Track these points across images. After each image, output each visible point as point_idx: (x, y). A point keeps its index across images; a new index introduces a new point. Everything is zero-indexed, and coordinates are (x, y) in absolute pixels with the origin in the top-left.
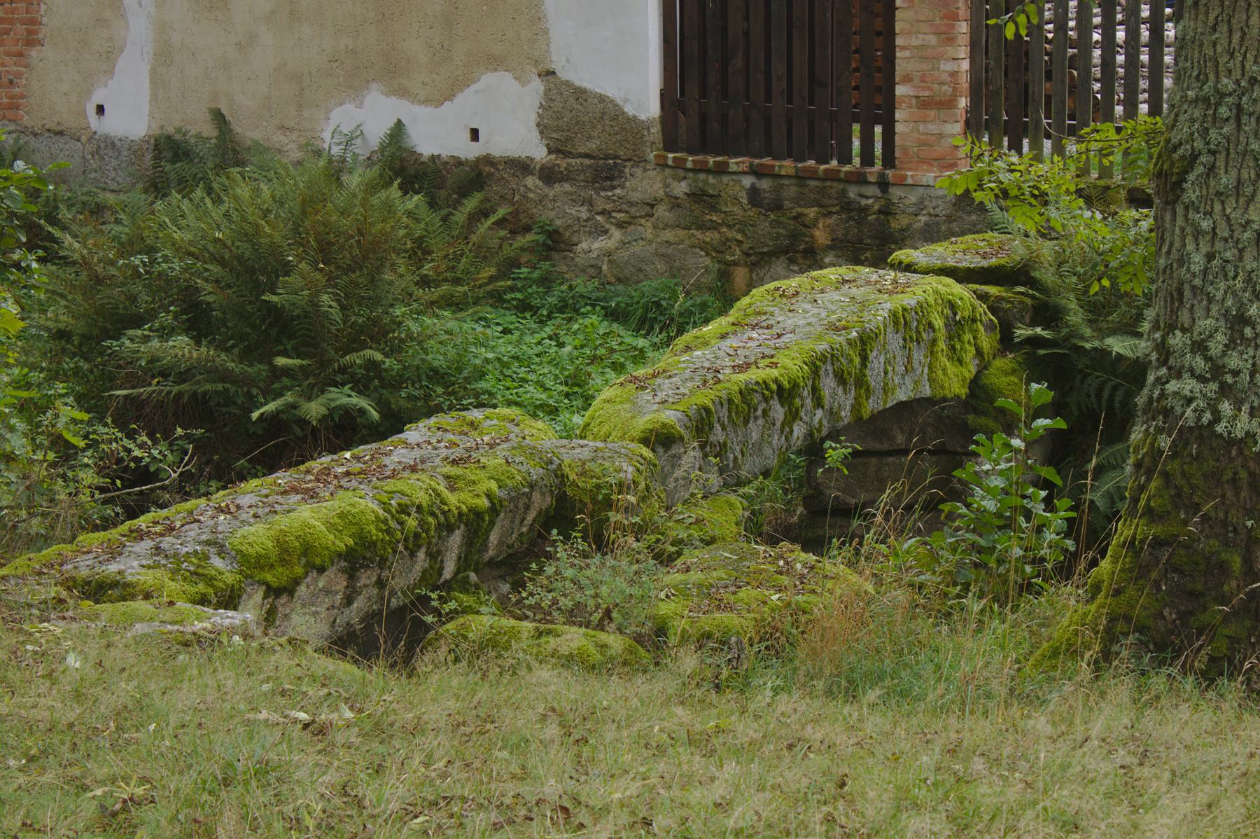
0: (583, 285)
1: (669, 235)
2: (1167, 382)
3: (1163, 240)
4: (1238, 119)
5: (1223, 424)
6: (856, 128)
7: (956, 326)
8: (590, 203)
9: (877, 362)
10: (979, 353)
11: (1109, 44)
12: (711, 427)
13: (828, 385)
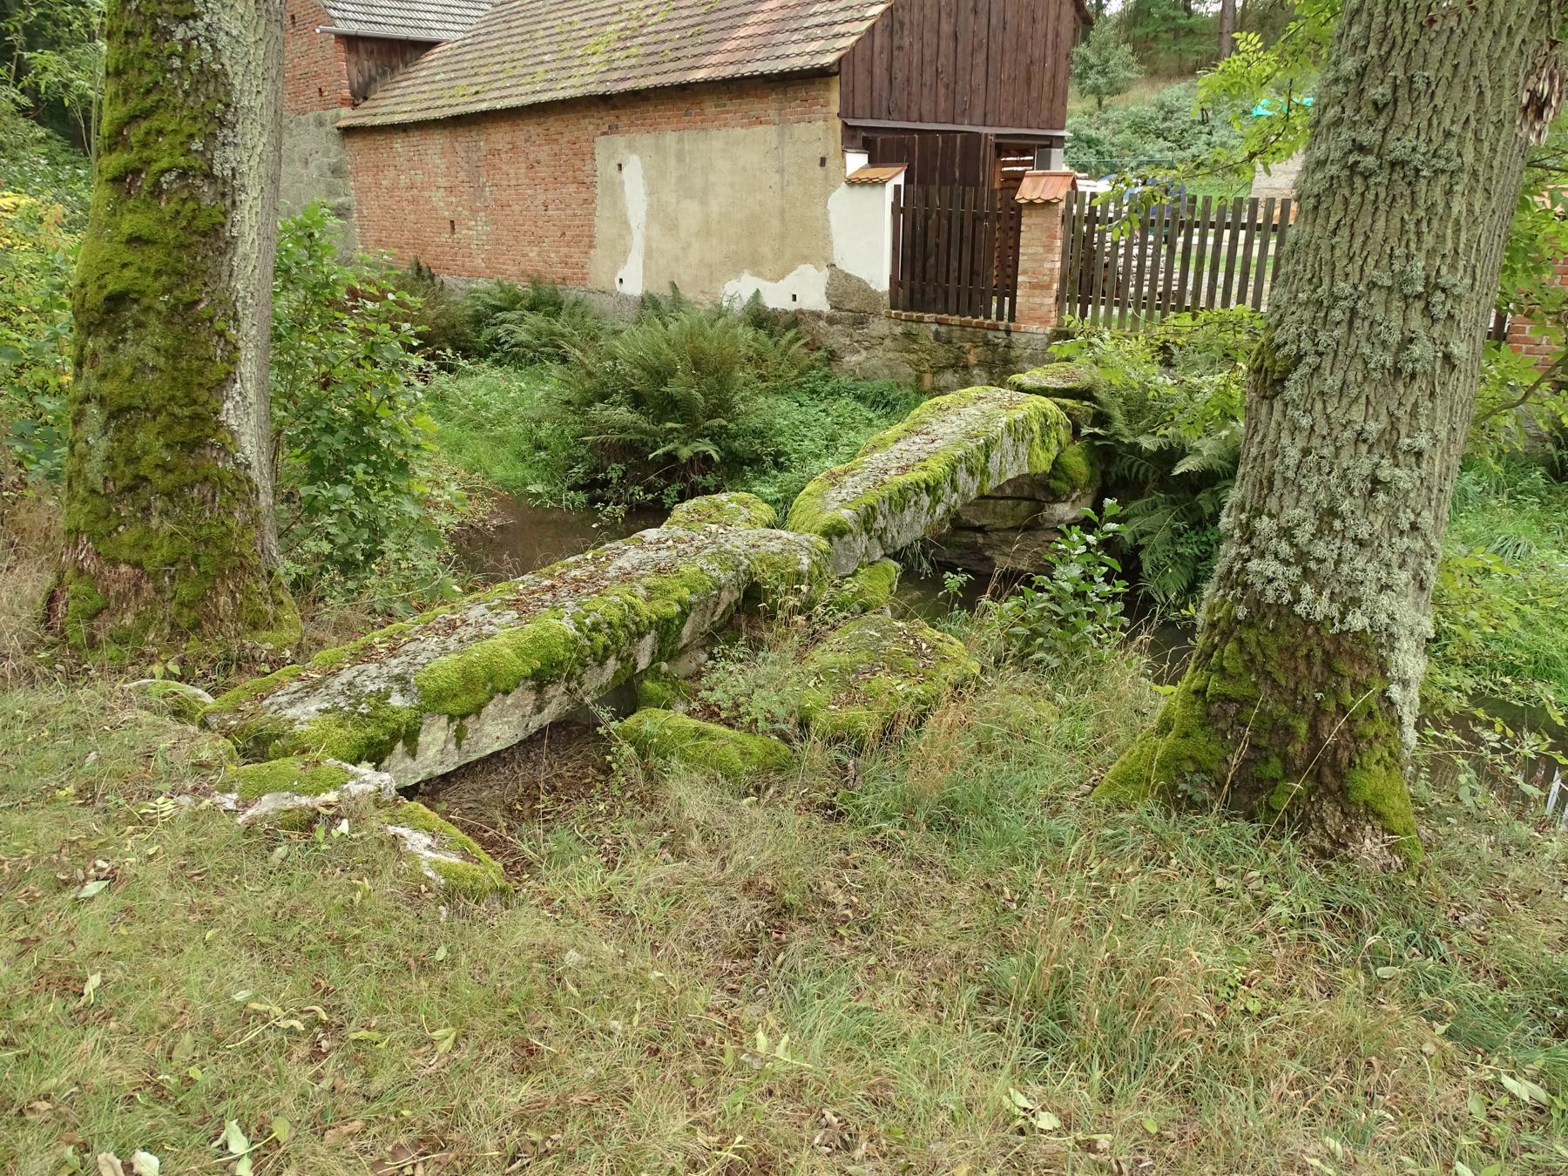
0: (845, 380)
1: (891, 355)
2: (1249, 560)
3: (1256, 430)
4: (1351, 323)
5: (1303, 605)
6: (995, 298)
7: (1046, 428)
8: (851, 336)
9: (995, 456)
10: (1059, 443)
11: (1128, 256)
12: (875, 519)
13: (962, 476)
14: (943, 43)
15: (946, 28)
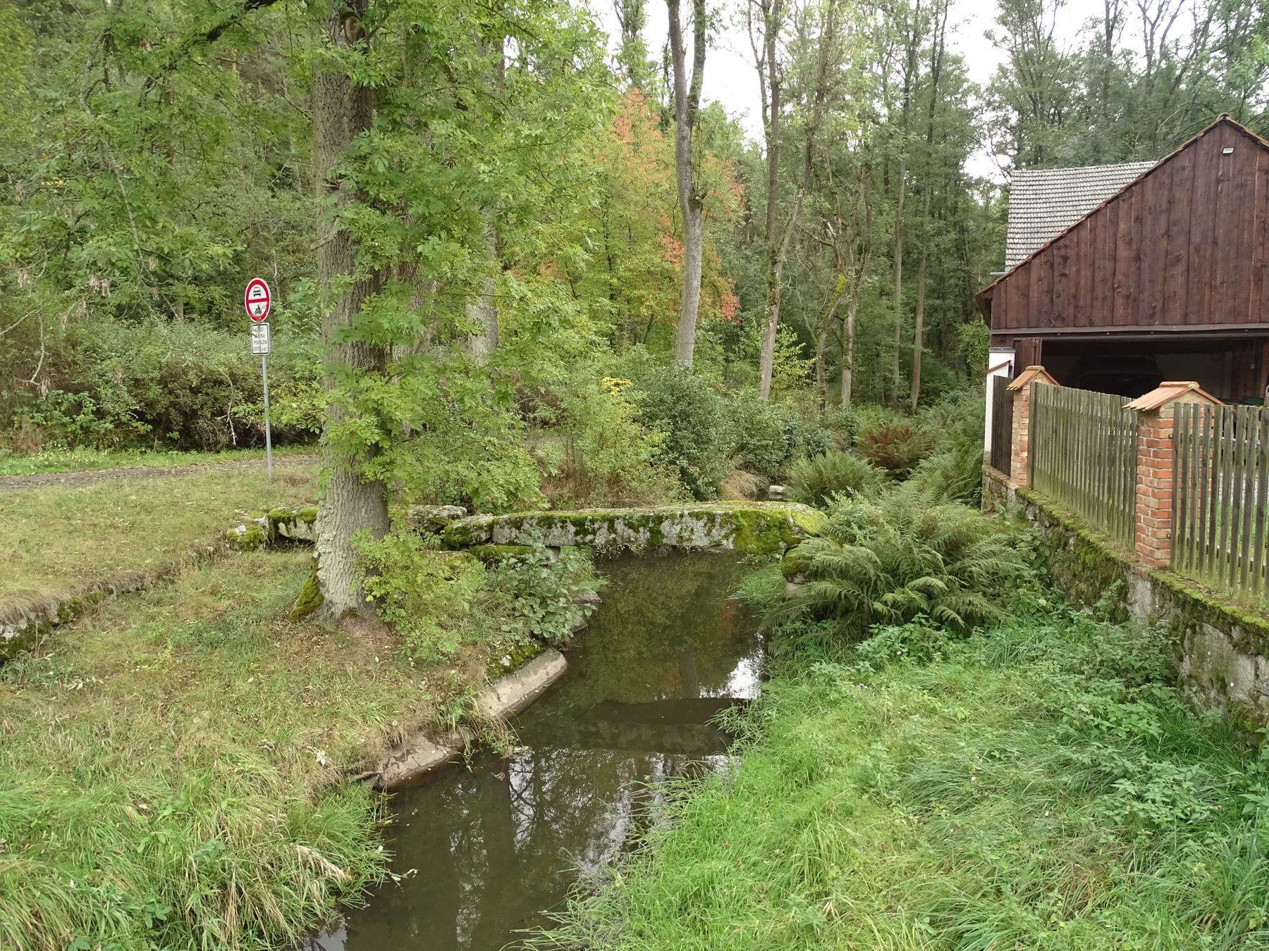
14: (1121, 267)
15: (1123, 252)
